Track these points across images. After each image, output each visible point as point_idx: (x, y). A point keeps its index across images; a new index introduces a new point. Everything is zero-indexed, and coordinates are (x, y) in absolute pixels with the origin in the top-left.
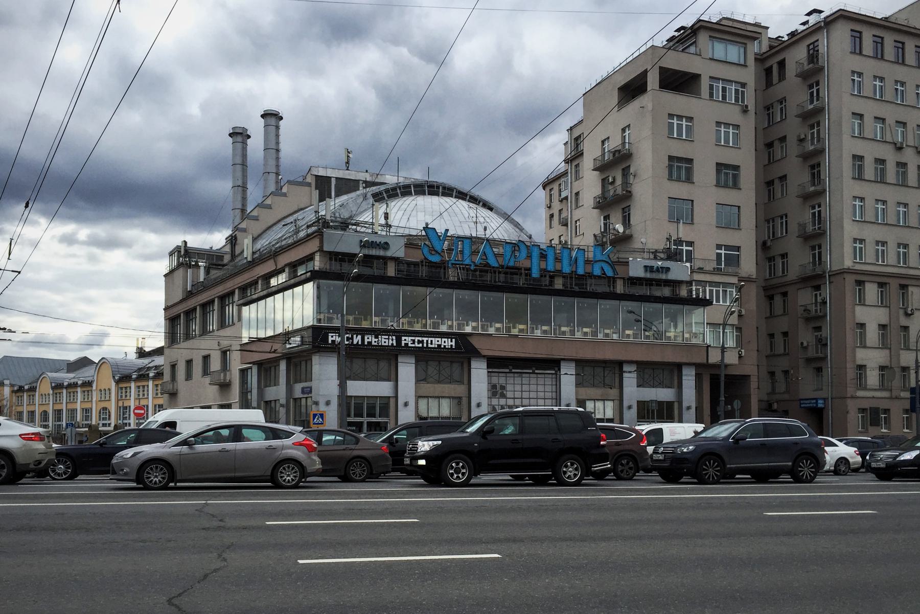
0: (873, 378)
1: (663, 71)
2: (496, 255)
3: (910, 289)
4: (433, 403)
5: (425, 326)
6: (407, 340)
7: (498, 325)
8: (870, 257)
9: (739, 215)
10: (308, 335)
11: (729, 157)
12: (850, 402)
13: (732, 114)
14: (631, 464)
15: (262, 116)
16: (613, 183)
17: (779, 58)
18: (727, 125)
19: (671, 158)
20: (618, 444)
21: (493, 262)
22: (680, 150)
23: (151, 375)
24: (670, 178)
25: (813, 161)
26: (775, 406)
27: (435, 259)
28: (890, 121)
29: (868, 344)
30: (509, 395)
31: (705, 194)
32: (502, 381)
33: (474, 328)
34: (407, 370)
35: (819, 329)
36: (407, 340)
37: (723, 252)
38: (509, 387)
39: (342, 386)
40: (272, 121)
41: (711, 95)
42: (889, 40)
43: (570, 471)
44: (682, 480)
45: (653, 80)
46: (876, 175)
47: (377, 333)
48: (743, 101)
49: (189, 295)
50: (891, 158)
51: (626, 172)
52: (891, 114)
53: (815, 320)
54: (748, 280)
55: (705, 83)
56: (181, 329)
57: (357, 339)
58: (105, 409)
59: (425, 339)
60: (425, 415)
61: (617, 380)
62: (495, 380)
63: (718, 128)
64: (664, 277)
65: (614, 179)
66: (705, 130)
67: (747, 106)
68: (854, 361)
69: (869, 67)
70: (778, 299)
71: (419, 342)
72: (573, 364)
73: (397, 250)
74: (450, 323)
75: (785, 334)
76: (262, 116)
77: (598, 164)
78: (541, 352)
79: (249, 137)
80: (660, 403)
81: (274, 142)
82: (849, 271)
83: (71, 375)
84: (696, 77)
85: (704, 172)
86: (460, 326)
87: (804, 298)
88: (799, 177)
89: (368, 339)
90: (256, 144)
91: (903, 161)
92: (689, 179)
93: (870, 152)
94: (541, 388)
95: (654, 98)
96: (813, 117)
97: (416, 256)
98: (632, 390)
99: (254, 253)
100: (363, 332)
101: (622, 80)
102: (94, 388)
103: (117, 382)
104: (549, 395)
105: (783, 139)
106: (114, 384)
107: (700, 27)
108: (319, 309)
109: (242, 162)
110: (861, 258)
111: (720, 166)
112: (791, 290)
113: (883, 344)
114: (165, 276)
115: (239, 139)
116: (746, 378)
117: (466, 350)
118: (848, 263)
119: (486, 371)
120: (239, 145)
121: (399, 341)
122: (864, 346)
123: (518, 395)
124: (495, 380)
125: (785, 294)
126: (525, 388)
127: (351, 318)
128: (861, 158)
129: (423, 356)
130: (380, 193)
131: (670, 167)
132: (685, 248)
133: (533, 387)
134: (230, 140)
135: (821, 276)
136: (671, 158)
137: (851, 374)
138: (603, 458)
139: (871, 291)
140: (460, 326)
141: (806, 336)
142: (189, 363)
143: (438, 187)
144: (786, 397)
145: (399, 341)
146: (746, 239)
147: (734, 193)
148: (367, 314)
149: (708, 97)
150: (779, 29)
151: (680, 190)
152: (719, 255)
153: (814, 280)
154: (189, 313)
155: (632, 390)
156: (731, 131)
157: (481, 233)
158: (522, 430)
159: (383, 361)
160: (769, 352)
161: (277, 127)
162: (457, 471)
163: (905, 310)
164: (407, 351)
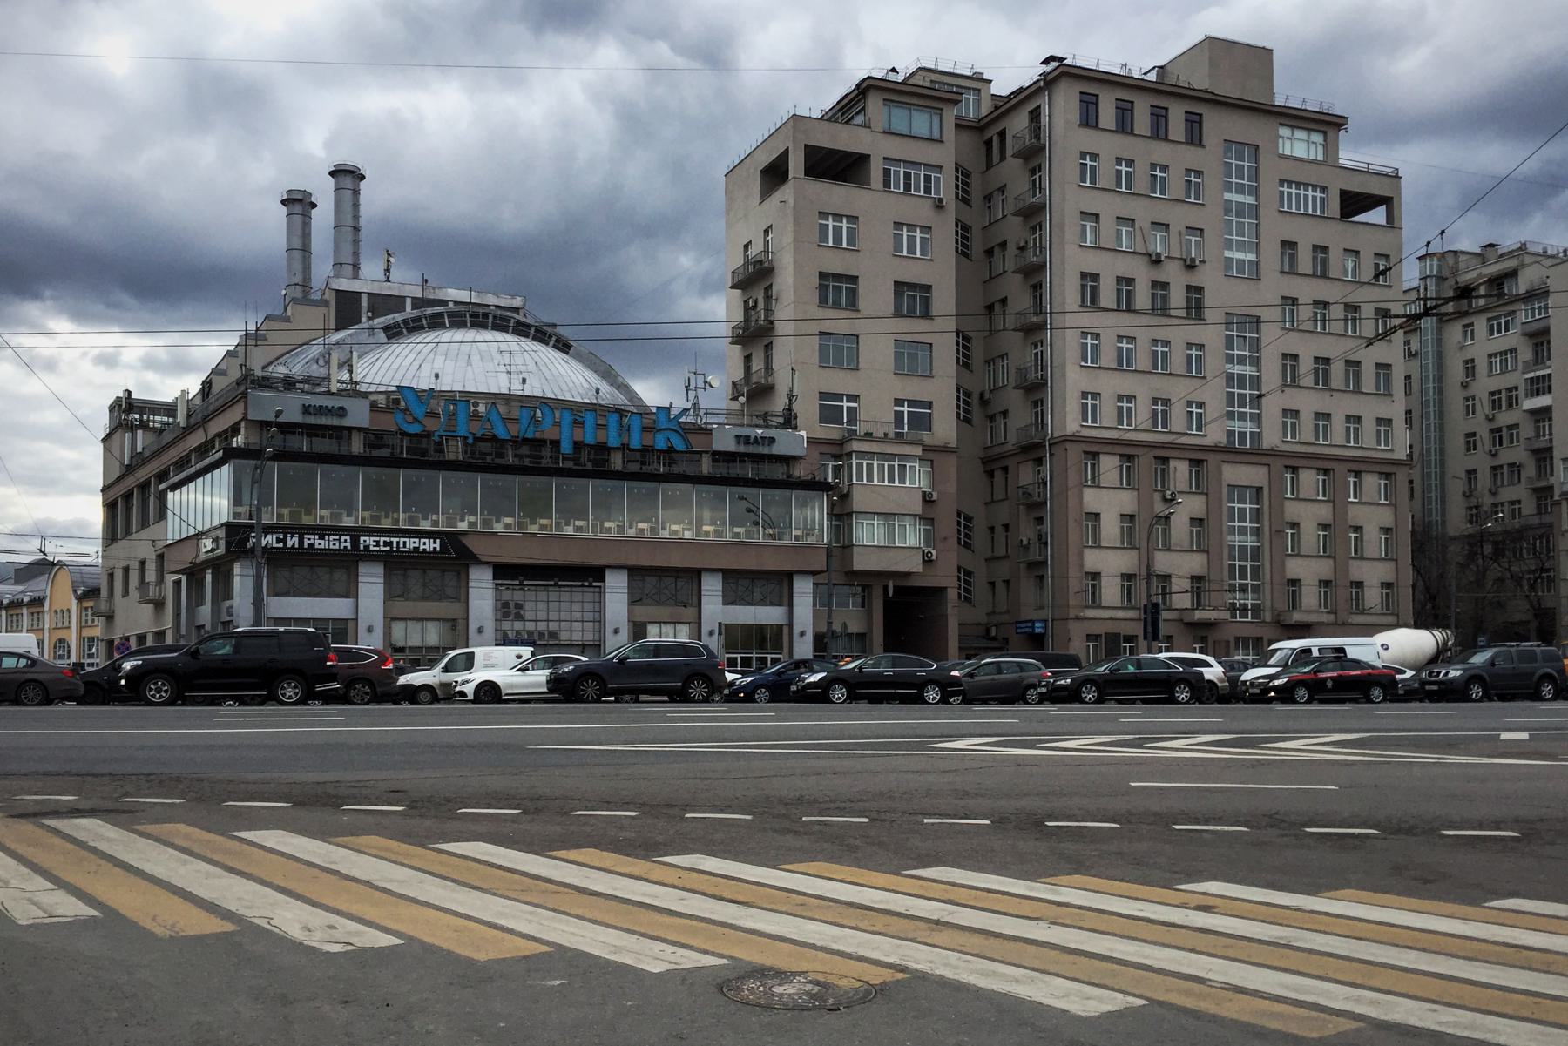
0: (1111, 591)
2: (506, 421)
3: (1172, 463)
4: (414, 628)
5: (397, 521)
6: (368, 541)
7: (508, 520)
8: (1107, 416)
10: (222, 534)
11: (914, 273)
12: (1072, 626)
13: (919, 210)
14: (367, 689)
15: (332, 174)
16: (755, 307)
18: (912, 227)
19: (823, 276)
20: (351, 667)
21: (501, 432)
22: (835, 264)
24: (823, 302)
25: (1034, 275)
26: (993, 632)
27: (414, 429)
28: (1143, 222)
29: (1103, 544)
30: (529, 615)
32: (518, 596)
33: (472, 524)
34: (371, 585)
35: (1040, 520)
36: (368, 541)
37: (905, 409)
38: (528, 606)
40: (348, 182)
41: (887, 184)
43: (289, 692)
45: (796, 165)
46: (1314, 267)
47: (322, 531)
48: (937, 192)
49: (129, 470)
50: (1143, 276)
52: (1142, 211)
53: (1035, 507)
54: (945, 450)
55: (876, 171)
57: (293, 541)
58: (61, 641)
59: (395, 540)
60: (400, 644)
61: (695, 599)
62: (507, 595)
63: (898, 233)
64: (766, 450)
65: (756, 302)
67: (941, 200)
68: (1082, 566)
69: (1108, 145)
70: (998, 474)
71: (386, 544)
72: (720, 576)
73: (358, 415)
74: (472, 519)
75: (1006, 527)
76: (332, 174)
78: (574, 558)
79: (314, 206)
80: (761, 628)
81: (349, 217)
82: (1074, 439)
83: (19, 588)
84: (863, 159)
85: (876, 296)
86: (451, 521)
87: (1025, 475)
88: (1020, 300)
89: (309, 539)
90: (323, 216)
91: (1163, 279)
92: (853, 304)
93: (1109, 269)
94: (576, 607)
95: (799, 188)
96: (1033, 214)
97: (388, 423)
98: (715, 608)
99: (189, 416)
100: (302, 530)
101: (765, 159)
102: (47, 608)
103: (80, 599)
104: (590, 616)
105: (1003, 245)
106: (74, 602)
107: (866, 88)
108: (237, 500)
109: (301, 247)
110: (1094, 421)
112: (1011, 463)
113: (1130, 543)
114: (104, 440)
115: (298, 208)
116: (940, 591)
117: (456, 555)
118: (1072, 425)
119: (491, 585)
120: (298, 219)
121: (355, 542)
122: (1097, 545)
123: (542, 616)
124: (507, 595)
125: (1005, 469)
126: (553, 606)
127: (285, 511)
129: (394, 563)
130: (396, 325)
131: (823, 288)
132: (845, 404)
133: (565, 606)
135: (1041, 445)
136: (823, 276)
137: (1074, 584)
138: (331, 676)
139: (1109, 465)
140: (451, 521)
141: (1027, 533)
142: (126, 570)
143: (485, 316)
144: (1006, 618)
145: (355, 542)
146: (941, 390)
147: (922, 325)
148: (309, 506)
149: (881, 187)
150: (1003, 84)
151: (840, 323)
152: (899, 415)
153: (1033, 450)
154: (128, 496)
155: (715, 608)
156: (918, 235)
157: (517, 388)
158: (236, 649)
159: (336, 570)
160: (989, 554)
161: (356, 192)
162: (158, 691)
163: (1163, 493)
164: (370, 556)
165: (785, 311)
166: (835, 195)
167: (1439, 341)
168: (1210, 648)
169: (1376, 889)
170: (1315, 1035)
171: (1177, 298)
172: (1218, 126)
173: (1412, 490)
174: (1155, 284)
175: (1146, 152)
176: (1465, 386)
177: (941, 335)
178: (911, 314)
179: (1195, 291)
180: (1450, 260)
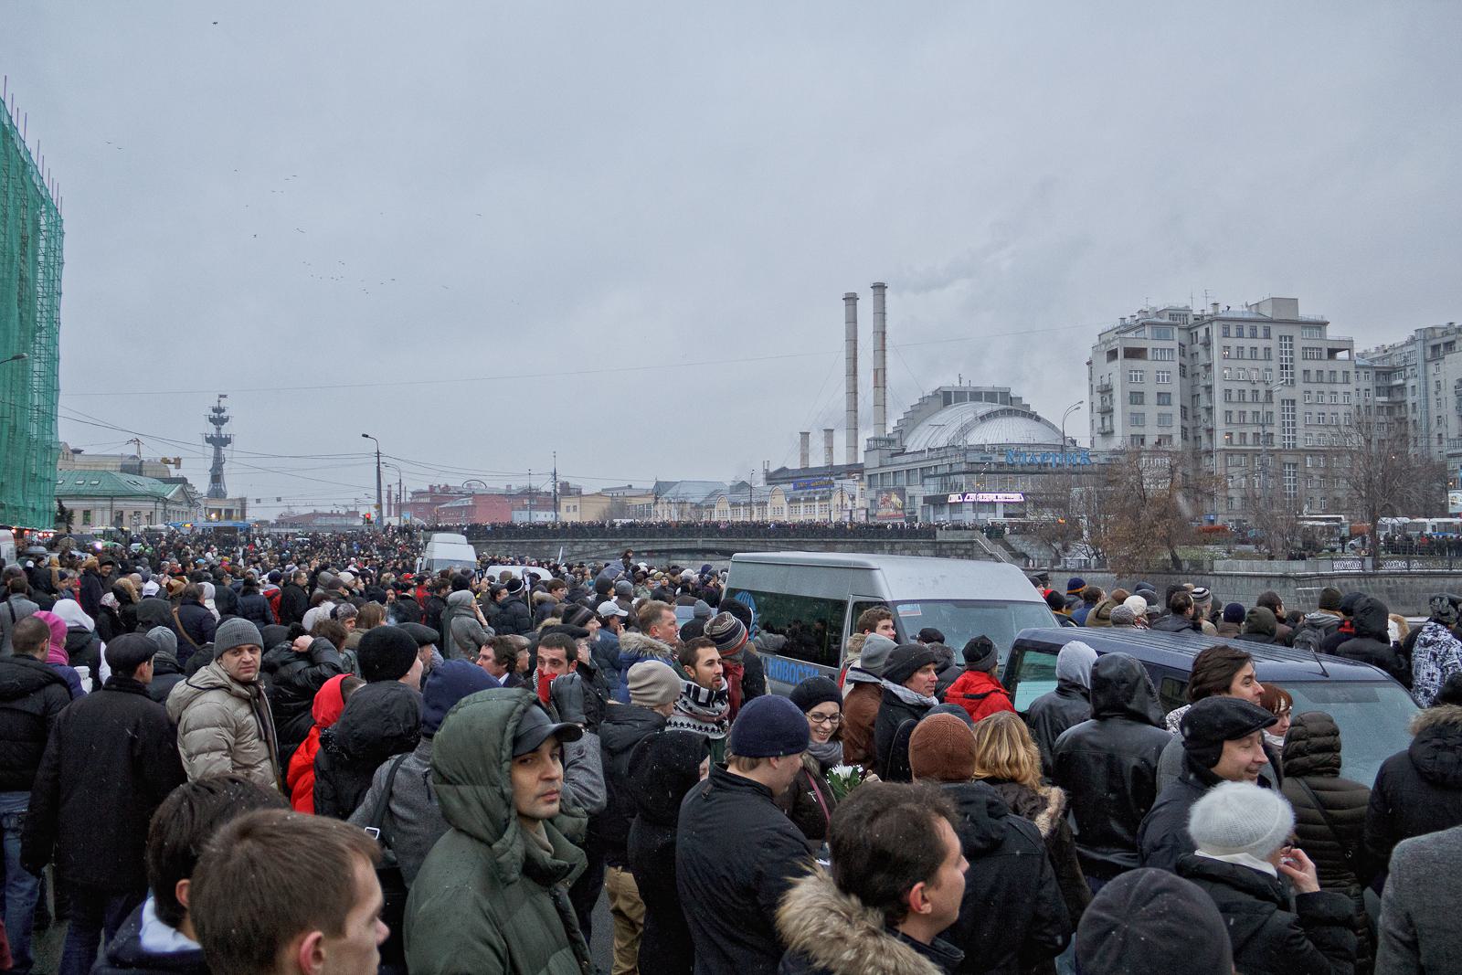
22: (1162, 389)
23: (817, 498)
31: (1151, 409)
39: (951, 516)
51: (1111, 396)
56: (1340, 969)
63: (1161, 372)
85: (1151, 399)
93: (1235, 387)
103: (789, 503)
111: (1159, 394)
134: (844, 302)
151: (1137, 409)
165: (1117, 407)
166: (1138, 364)
167: (1426, 371)
168: (1399, 510)
171: (1262, 396)
172: (1276, 331)
175: (1247, 343)
176: (1436, 393)
177: (1175, 409)
178: (1163, 404)
180: (1430, 333)
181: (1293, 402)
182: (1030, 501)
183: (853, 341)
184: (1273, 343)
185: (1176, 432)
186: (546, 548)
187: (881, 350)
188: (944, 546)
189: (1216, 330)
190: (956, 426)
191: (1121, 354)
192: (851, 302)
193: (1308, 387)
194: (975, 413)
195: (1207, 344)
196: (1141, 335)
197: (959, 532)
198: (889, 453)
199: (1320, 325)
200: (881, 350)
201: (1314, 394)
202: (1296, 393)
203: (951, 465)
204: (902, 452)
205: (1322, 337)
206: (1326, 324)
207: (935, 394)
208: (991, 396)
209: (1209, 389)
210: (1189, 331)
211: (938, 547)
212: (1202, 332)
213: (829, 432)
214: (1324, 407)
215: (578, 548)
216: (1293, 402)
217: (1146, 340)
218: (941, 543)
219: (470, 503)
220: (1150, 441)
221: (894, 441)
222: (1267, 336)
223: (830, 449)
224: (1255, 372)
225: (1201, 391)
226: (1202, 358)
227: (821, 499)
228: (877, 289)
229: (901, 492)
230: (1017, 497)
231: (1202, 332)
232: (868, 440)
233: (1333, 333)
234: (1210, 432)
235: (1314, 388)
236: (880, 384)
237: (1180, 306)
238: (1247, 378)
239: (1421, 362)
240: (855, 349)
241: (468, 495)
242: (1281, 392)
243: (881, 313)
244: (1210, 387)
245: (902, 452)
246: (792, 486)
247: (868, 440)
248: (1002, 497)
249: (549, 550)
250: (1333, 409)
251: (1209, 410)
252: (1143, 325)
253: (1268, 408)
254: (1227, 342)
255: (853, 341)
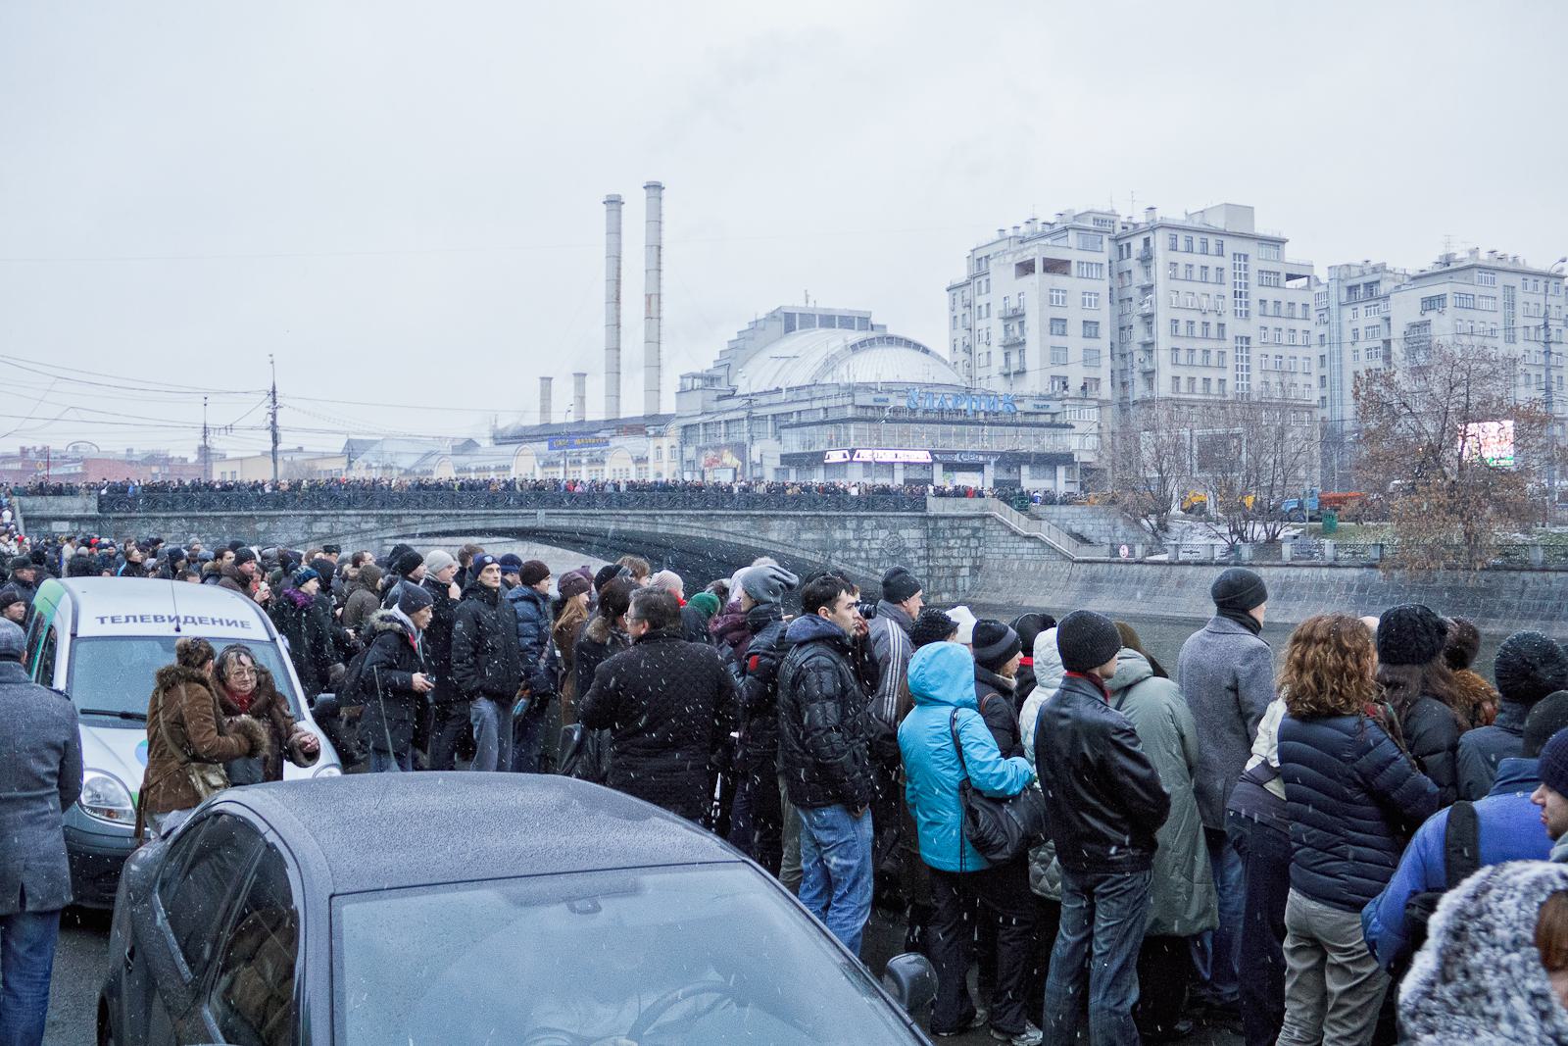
1: (1046, 260)
9: (104, 745)
11: (1090, 316)
17: (1127, 241)
22: (1059, 313)
31: (1075, 342)
42: (1197, 239)
44: (1088, 830)
51: (1022, 324)
55: (1074, 265)
63: (1085, 293)
66: (1075, 299)
77: (1003, 315)
84: (1068, 262)
85: (1075, 328)
128: (1177, 321)
151: (1059, 341)
161: (620, 211)
166: (1058, 280)
169: (739, 848)
170: (1013, 759)
171: (1213, 331)
172: (1231, 246)
173: (59, 491)
174: (1219, 325)
175: (1197, 260)
177: (1104, 343)
178: (1090, 337)
179: (1221, 326)
181: (1248, 339)
182: (940, 462)
183: (615, 259)
184: (1226, 262)
185: (1104, 374)
186: (261, 527)
187: (656, 269)
188: (941, 524)
189: (1160, 241)
190: (817, 358)
191: (1039, 266)
192: (614, 206)
193: (1265, 322)
194: (845, 341)
195: (1146, 260)
196: (1061, 242)
197: (963, 500)
198: (715, 395)
199: (1278, 243)
200: (656, 269)
201: (1271, 331)
202: (1250, 329)
203: (826, 409)
204: (732, 395)
205: (1279, 259)
206: (1283, 242)
207: (772, 316)
208: (847, 322)
209: (1148, 319)
210: (1125, 244)
211: (931, 524)
212: (1137, 244)
213: (580, 377)
214: (1281, 348)
215: (321, 527)
216: (1248, 339)
217: (1067, 249)
218: (936, 518)
219: (79, 470)
220: (1075, 384)
221: (719, 379)
222: (1220, 254)
223: (581, 399)
224: (1205, 299)
225: (1136, 321)
226: (1139, 277)
227: (591, 462)
228: (651, 190)
229: (740, 450)
230: (923, 456)
231: (1137, 244)
232: (682, 377)
233: (1292, 254)
234: (1149, 376)
235: (1271, 323)
236: (654, 314)
237: (1105, 210)
238: (1196, 306)
239: (1334, 306)
240: (619, 269)
241: (75, 461)
242: (1235, 327)
243: (655, 221)
244: (1151, 315)
245: (732, 395)
246: (545, 445)
247: (682, 377)
248: (905, 456)
249: (267, 531)
250: (1291, 351)
251: (1148, 347)
252: (1066, 229)
253: (1222, 346)
254: (1174, 256)
255: (615, 259)
